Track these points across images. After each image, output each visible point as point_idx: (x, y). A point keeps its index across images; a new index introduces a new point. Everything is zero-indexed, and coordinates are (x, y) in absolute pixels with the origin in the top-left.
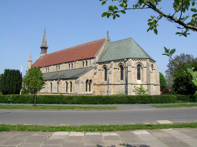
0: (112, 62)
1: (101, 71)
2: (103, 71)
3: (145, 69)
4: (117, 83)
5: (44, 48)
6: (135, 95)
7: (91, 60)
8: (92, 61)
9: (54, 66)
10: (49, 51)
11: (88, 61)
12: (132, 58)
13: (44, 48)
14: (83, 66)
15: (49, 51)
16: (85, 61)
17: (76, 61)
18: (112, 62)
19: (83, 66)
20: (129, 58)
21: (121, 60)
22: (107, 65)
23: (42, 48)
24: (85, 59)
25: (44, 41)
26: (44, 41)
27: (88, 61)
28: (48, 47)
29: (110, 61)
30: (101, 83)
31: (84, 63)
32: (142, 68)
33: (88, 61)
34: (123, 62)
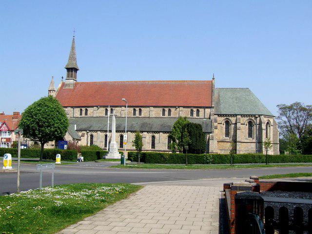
0: (239, 117)
1: (222, 125)
2: (246, 125)
3: (272, 127)
4: (245, 141)
5: (72, 70)
6: (273, 154)
7: (206, 110)
8: (208, 111)
9: (186, 109)
10: (81, 77)
11: (200, 110)
12: (242, 115)
13: (72, 70)
14: (81, 114)
15: (82, 77)
16: (195, 110)
17: (179, 107)
18: (239, 117)
19: (81, 114)
20: (238, 115)
21: (252, 115)
22: (230, 118)
23: (76, 70)
24: (195, 107)
25: (72, 57)
26: (72, 57)
27: (173, 110)
28: (79, 68)
29: (236, 115)
30: (221, 139)
31: (194, 113)
32: (269, 126)
33: (200, 110)
34: (253, 118)
